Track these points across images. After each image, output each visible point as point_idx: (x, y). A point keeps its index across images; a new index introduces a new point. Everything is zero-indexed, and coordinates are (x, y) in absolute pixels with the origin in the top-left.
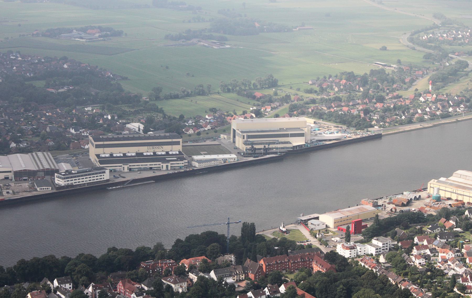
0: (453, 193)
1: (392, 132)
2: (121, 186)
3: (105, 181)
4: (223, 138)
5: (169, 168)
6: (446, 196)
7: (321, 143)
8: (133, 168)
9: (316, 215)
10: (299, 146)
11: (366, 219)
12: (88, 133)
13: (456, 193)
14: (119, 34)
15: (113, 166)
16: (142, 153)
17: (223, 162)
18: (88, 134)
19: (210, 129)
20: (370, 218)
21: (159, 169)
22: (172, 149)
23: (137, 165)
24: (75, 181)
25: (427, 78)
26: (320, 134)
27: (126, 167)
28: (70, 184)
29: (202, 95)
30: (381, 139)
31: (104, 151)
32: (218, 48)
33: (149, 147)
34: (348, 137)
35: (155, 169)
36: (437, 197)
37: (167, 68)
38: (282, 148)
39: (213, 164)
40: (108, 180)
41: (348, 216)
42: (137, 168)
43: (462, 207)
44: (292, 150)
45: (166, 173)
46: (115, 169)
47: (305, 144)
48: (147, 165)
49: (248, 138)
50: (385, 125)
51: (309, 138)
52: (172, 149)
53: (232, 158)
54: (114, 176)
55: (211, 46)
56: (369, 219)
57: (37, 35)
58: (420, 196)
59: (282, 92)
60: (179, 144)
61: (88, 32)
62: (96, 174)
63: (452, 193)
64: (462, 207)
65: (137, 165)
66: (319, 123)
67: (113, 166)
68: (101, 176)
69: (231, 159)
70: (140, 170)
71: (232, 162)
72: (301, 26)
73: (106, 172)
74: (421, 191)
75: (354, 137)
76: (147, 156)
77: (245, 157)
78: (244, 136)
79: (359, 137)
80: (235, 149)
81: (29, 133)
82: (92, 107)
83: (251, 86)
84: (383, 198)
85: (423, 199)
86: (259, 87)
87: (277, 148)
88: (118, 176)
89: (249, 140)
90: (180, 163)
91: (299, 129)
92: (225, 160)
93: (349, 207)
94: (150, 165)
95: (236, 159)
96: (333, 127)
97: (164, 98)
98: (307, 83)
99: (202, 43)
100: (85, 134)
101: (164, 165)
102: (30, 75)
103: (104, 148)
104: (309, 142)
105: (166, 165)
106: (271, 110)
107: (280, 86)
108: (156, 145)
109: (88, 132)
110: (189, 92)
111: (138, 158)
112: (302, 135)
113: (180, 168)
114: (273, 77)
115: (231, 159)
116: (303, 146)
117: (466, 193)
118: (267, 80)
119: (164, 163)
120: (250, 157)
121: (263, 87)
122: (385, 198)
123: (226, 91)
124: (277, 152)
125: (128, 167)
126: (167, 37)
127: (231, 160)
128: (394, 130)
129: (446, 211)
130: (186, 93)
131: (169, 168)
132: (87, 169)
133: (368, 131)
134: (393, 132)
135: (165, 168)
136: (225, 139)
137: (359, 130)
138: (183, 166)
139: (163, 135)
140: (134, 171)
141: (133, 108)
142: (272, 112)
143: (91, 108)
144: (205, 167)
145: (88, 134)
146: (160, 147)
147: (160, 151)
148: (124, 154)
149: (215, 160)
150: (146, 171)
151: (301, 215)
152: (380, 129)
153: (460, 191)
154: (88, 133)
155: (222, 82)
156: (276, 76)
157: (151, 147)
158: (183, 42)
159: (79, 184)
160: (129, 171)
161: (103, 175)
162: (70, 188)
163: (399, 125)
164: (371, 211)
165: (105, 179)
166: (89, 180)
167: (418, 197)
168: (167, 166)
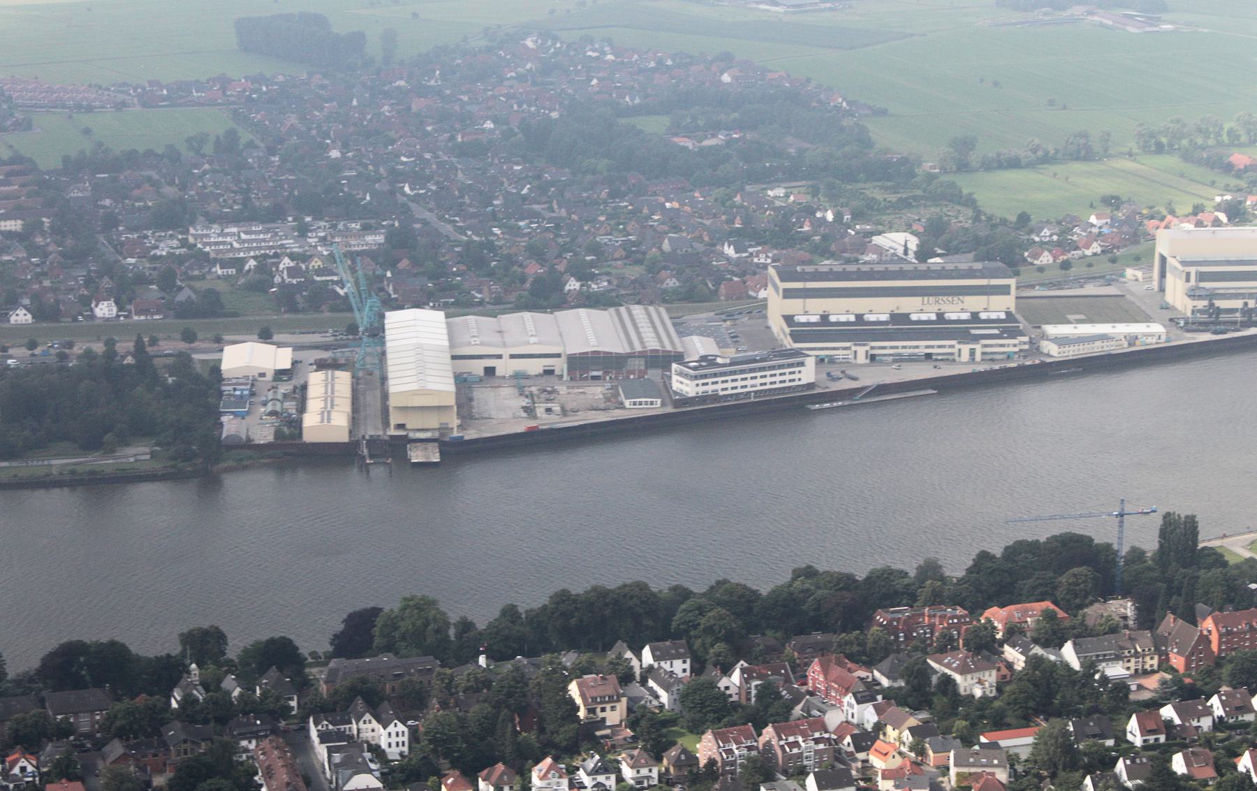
2: (847, 403)
3: (803, 386)
4: (1134, 278)
5: (978, 357)
8: (879, 355)
15: (827, 349)
19: (1099, 252)
21: (950, 359)
23: (892, 348)
24: (725, 385)
27: (861, 350)
28: (710, 393)
32: (1141, 31)
33: (926, 298)
35: (940, 357)
40: (810, 386)
42: (890, 355)
46: (831, 356)
48: (917, 347)
53: (1152, 335)
54: (829, 374)
60: (1008, 293)
65: (892, 348)
67: (827, 349)
68: (794, 373)
69: (1150, 336)
70: (899, 360)
77: (1188, 331)
78: (1188, 274)
80: (1162, 308)
86: (1244, 138)
89: (1202, 284)
90: (1009, 345)
92: (1133, 339)
94: (927, 347)
99: (1096, 18)
100: (762, 261)
101: (966, 349)
102: (632, 99)
108: (948, 295)
113: (1009, 357)
115: (1150, 336)
119: (964, 343)
123: (1153, 148)
125: (867, 352)
130: (1040, 153)
131: (978, 357)
132: (756, 355)
135: (965, 356)
136: (1137, 280)
138: (1015, 353)
141: (895, 193)
146: (956, 298)
147: (956, 310)
148: (859, 317)
149: (1103, 337)
157: (931, 298)
158: (1046, 14)
161: (800, 372)
165: (803, 382)
168: (972, 352)
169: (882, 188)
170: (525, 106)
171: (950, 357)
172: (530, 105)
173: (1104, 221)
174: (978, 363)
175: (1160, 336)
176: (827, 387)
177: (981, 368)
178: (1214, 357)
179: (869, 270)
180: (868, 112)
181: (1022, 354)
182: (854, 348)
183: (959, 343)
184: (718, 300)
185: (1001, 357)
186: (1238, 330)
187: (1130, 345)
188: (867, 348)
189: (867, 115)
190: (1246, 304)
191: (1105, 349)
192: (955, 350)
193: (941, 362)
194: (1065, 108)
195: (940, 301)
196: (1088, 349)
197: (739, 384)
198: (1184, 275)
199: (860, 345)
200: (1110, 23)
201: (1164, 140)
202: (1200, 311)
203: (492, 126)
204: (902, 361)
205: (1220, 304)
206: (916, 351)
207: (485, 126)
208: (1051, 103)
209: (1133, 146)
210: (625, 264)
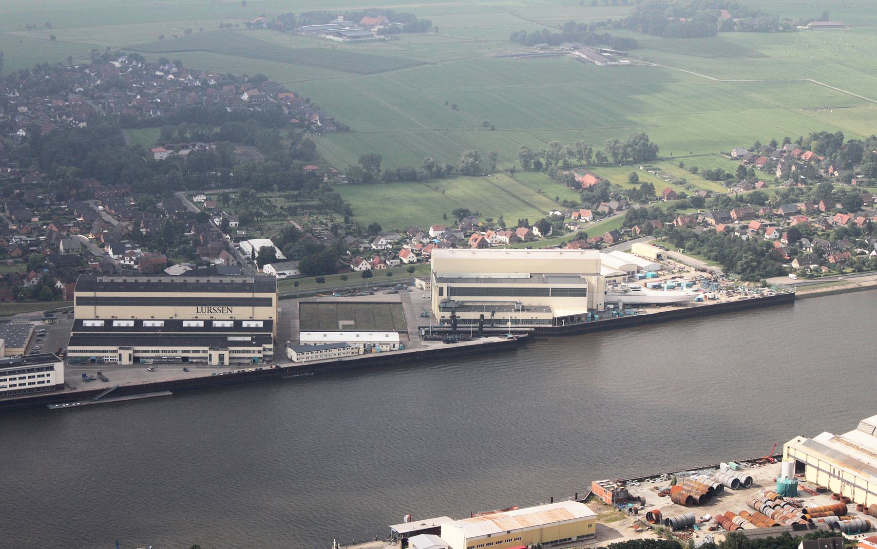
0: (834, 476)
1: (825, 290)
2: (85, 403)
3: (52, 387)
4: (420, 287)
5: (227, 361)
6: (819, 483)
7: (632, 312)
8: (143, 358)
9: (430, 523)
10: (566, 318)
11: (566, 540)
12: (133, 260)
13: (839, 478)
14: (422, 27)
15: (97, 351)
16: (180, 322)
17: (362, 351)
18: (132, 263)
19: (415, 260)
20: (578, 537)
21: (203, 363)
22: (253, 313)
23: (153, 351)
25: (43, 312)
26: (636, 289)
27: (125, 354)
29: (474, 176)
30: (793, 306)
31: (95, 313)
32: (604, 64)
33: (200, 308)
34: (709, 299)
35: (195, 361)
36: (786, 485)
37: (454, 109)
38: (525, 321)
39: (334, 355)
40: (58, 387)
41: (509, 532)
42: (152, 358)
43: (808, 527)
44: (551, 326)
45: (220, 372)
46: (100, 357)
47: (586, 314)
48: (175, 351)
49: (451, 295)
50: (821, 270)
51: (600, 300)
52: (253, 313)
53: (387, 344)
54: (84, 376)
55: (591, 60)
56: (574, 539)
57: (258, 25)
58: (749, 479)
59: (655, 174)
60: (271, 305)
61: (363, 21)
62: (29, 371)
63: (832, 477)
64: (808, 527)
65: (153, 351)
66: (668, 258)
67: (97, 351)
68: (43, 376)
69: (385, 344)
70: (159, 362)
71: (386, 351)
72: (820, 20)
73: (55, 368)
74: (769, 461)
75: (724, 299)
76: (190, 329)
77: (426, 339)
78: (441, 290)
79: (735, 298)
80: (422, 317)
81: (14, 254)
82: (206, 195)
83: (591, 158)
84: (658, 476)
85: (758, 486)
86: (611, 160)
87: (515, 321)
88: (95, 375)
89: (453, 298)
90: (254, 352)
91: (577, 277)
92: (368, 348)
93: (552, 502)
94: (184, 352)
95: (397, 346)
96: (694, 269)
97: (383, 180)
98: (727, 155)
99: (577, 53)
100: (127, 263)
101: (215, 354)
102: (154, 113)
103: (97, 307)
104: (601, 308)
105: (219, 355)
106: (594, 219)
107: (662, 160)
108: (219, 305)
109: (134, 258)
110: (441, 169)
111: (164, 335)
112: (581, 293)
113: (254, 361)
114: (647, 140)
115: (385, 344)
116: (583, 319)
117: (861, 479)
118: (629, 146)
119: (214, 349)
120: (436, 339)
121: (620, 162)
122: (665, 478)
123: (533, 167)
124: (507, 332)
125: (130, 355)
126: (518, 38)
127: (385, 347)
128: (833, 286)
129: (737, 543)
130: (434, 169)
131: (227, 361)
132: (10, 360)
133: (765, 285)
134: (830, 289)
135: (215, 361)
136: (422, 289)
137: (748, 280)
138: (260, 358)
139: (241, 282)
140: (145, 365)
141: (297, 201)
142: (592, 223)
143: (205, 198)
144: (307, 364)
145: (132, 263)
146: (225, 308)
147: (222, 319)
148: (139, 323)
149: (342, 345)
150: (171, 366)
151: (406, 517)
152: (799, 281)
153: (849, 474)
154: (133, 260)
155: (523, 148)
156: (653, 140)
157: (204, 308)
158: (542, 48)
159: (22, 390)
160: (132, 363)
161: (48, 375)
162: (347, 329)
163: (853, 271)
164: (579, 520)
165: (53, 383)
166: (11, 386)
167: (743, 480)
168: (221, 357)
169: (286, 197)
170: (64, 117)
171: (204, 361)
172: (68, 117)
173: (440, 232)
174: (227, 367)
175: (394, 345)
176: (75, 388)
177: (227, 371)
178: (369, 376)
179: (157, 281)
180: (334, 129)
181: (267, 359)
182: (120, 352)
183: (210, 349)
184: (62, 299)
185: (248, 361)
186: (469, 340)
187: (365, 352)
188: (131, 352)
189: (332, 131)
190: (482, 316)
191: (342, 355)
192: (207, 355)
193: (194, 366)
194: (493, 129)
195: (212, 310)
196: (324, 357)
197: (27, 381)
198: (438, 290)
199: (124, 349)
200: (585, 57)
201: (543, 161)
202: (447, 321)
203: (24, 134)
204: (161, 363)
205: (462, 315)
206: (174, 354)
207: (18, 133)
208: (486, 124)
209: (518, 164)
210: (17, 262)
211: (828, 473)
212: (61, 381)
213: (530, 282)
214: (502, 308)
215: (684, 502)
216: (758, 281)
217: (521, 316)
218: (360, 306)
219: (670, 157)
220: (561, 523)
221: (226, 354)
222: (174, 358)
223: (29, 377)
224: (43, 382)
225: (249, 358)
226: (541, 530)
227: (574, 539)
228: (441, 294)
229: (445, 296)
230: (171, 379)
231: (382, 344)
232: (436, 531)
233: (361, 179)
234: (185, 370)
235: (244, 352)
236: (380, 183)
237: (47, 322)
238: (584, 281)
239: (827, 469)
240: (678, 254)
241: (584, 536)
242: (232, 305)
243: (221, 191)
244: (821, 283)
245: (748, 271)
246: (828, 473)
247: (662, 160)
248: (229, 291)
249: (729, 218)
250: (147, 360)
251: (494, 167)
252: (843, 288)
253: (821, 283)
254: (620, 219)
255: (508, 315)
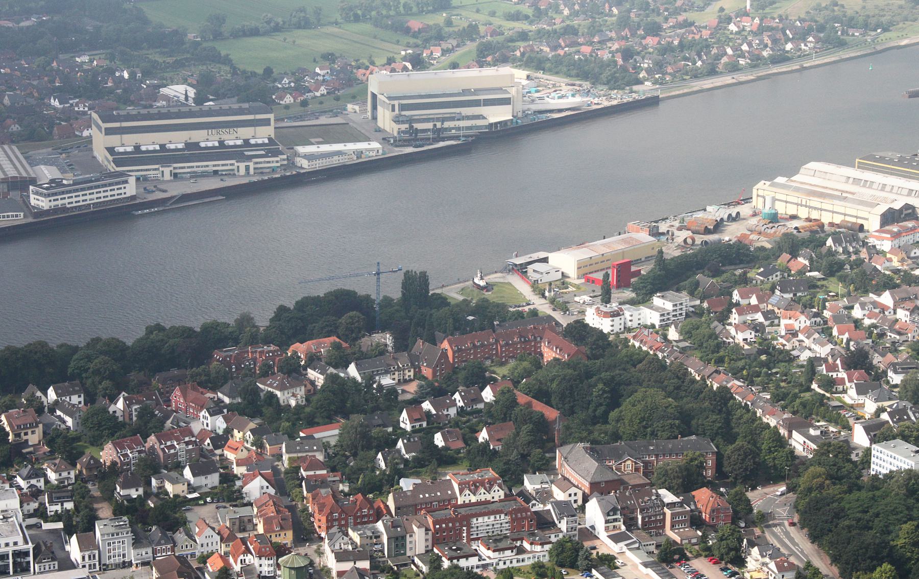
0: (802, 205)
1: (678, 93)
2: (161, 209)
5: (252, 171)
7: (544, 117)
8: (180, 173)
9: (542, 255)
13: (806, 206)
15: (142, 170)
18: (86, 109)
21: (231, 174)
23: (188, 167)
26: (541, 98)
27: (167, 171)
33: (210, 131)
38: (468, 128)
40: (133, 198)
41: (603, 255)
42: (188, 173)
48: (207, 166)
51: (520, 107)
53: (372, 150)
54: (145, 189)
56: (643, 259)
58: (738, 213)
60: (269, 125)
65: (188, 167)
67: (142, 170)
68: (121, 188)
70: (195, 176)
74: (739, 204)
77: (397, 146)
84: (667, 218)
85: (744, 219)
86: (415, 9)
87: (458, 129)
88: (153, 188)
89: (403, 113)
92: (359, 154)
94: (214, 166)
95: (381, 151)
97: (231, 35)
100: (81, 109)
101: (242, 166)
104: (520, 115)
106: (442, 55)
108: (226, 127)
112: (506, 102)
116: (509, 123)
121: (423, 11)
123: (352, 18)
125: (171, 171)
128: (683, 89)
131: (252, 171)
133: (632, 92)
134: (681, 92)
135: (242, 171)
138: (278, 167)
140: (182, 179)
145: (86, 109)
146: (231, 130)
147: (233, 139)
148: (163, 146)
149: (339, 153)
153: (815, 202)
160: (172, 178)
161: (125, 188)
163: (691, 78)
165: (128, 195)
167: (734, 215)
168: (247, 168)
171: (231, 173)
174: (252, 176)
185: (268, 170)
191: (341, 161)
197: (109, 193)
201: (359, 12)
205: (416, 126)
206: (207, 169)
211: (796, 204)
212: (134, 193)
213: (464, 96)
214: (443, 120)
215: (703, 232)
216: (623, 89)
217: (462, 124)
218: (315, 128)
219: (460, 5)
220: (635, 247)
221: (252, 165)
222: (206, 172)
223: (83, 195)
224: (121, 194)
225: (269, 168)
226: (623, 252)
227: (643, 259)
228: (393, 110)
229: (397, 111)
230: (213, 187)
231: (367, 150)
232: (545, 260)
233: (211, 37)
234: (222, 180)
235: (265, 162)
236: (228, 38)
237: (64, 155)
238: (506, 92)
239: (795, 200)
240: (540, 74)
241: (649, 257)
242: (237, 127)
243: (109, 51)
244: (672, 87)
245: (612, 82)
246: (796, 204)
247: (455, 8)
248: (228, 115)
249: (560, 46)
250: (184, 175)
251: (319, 20)
252: (691, 90)
253: (672, 87)
254: (470, 52)
255: (451, 124)
